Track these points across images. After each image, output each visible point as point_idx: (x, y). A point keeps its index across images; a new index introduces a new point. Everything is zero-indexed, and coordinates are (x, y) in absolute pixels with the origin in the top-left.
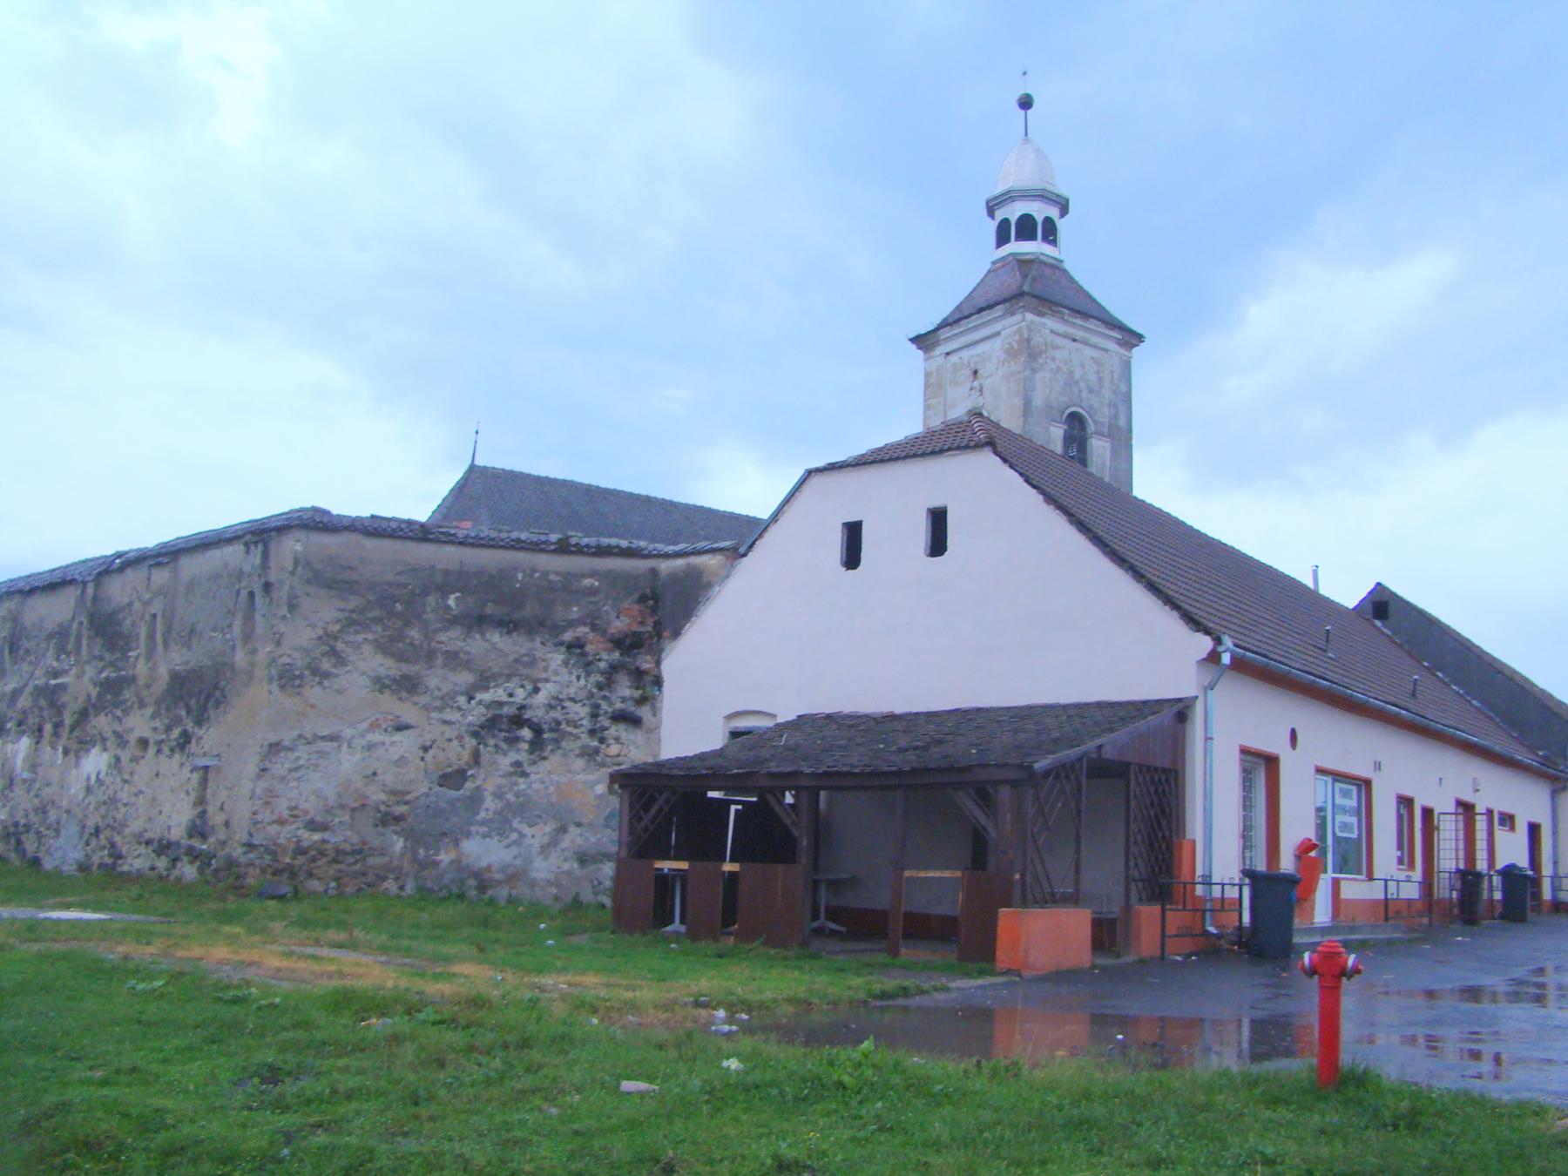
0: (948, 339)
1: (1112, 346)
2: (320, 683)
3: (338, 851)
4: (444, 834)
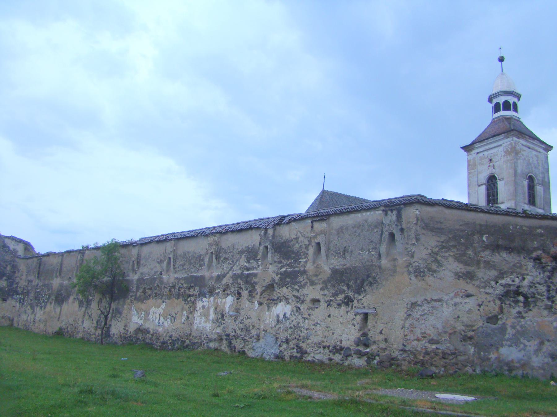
0: (477, 148)
1: (541, 150)
2: (432, 275)
3: (443, 353)
4: (492, 345)
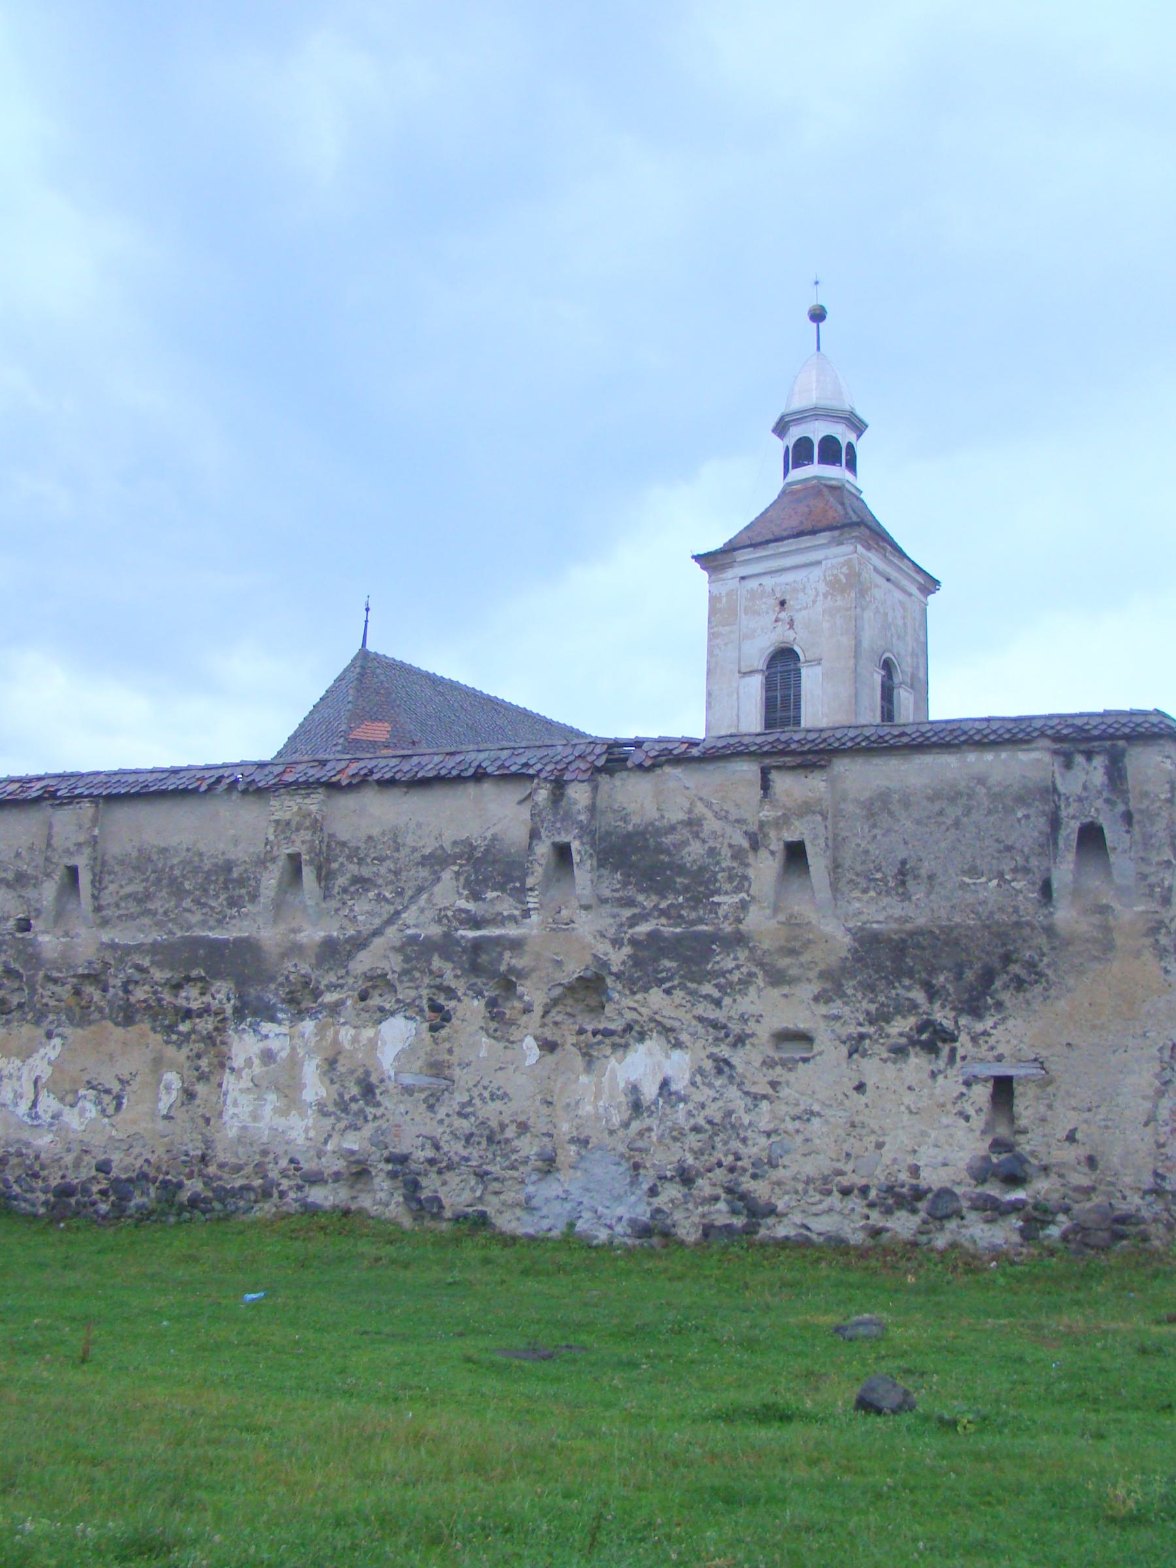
1: (914, 590)
